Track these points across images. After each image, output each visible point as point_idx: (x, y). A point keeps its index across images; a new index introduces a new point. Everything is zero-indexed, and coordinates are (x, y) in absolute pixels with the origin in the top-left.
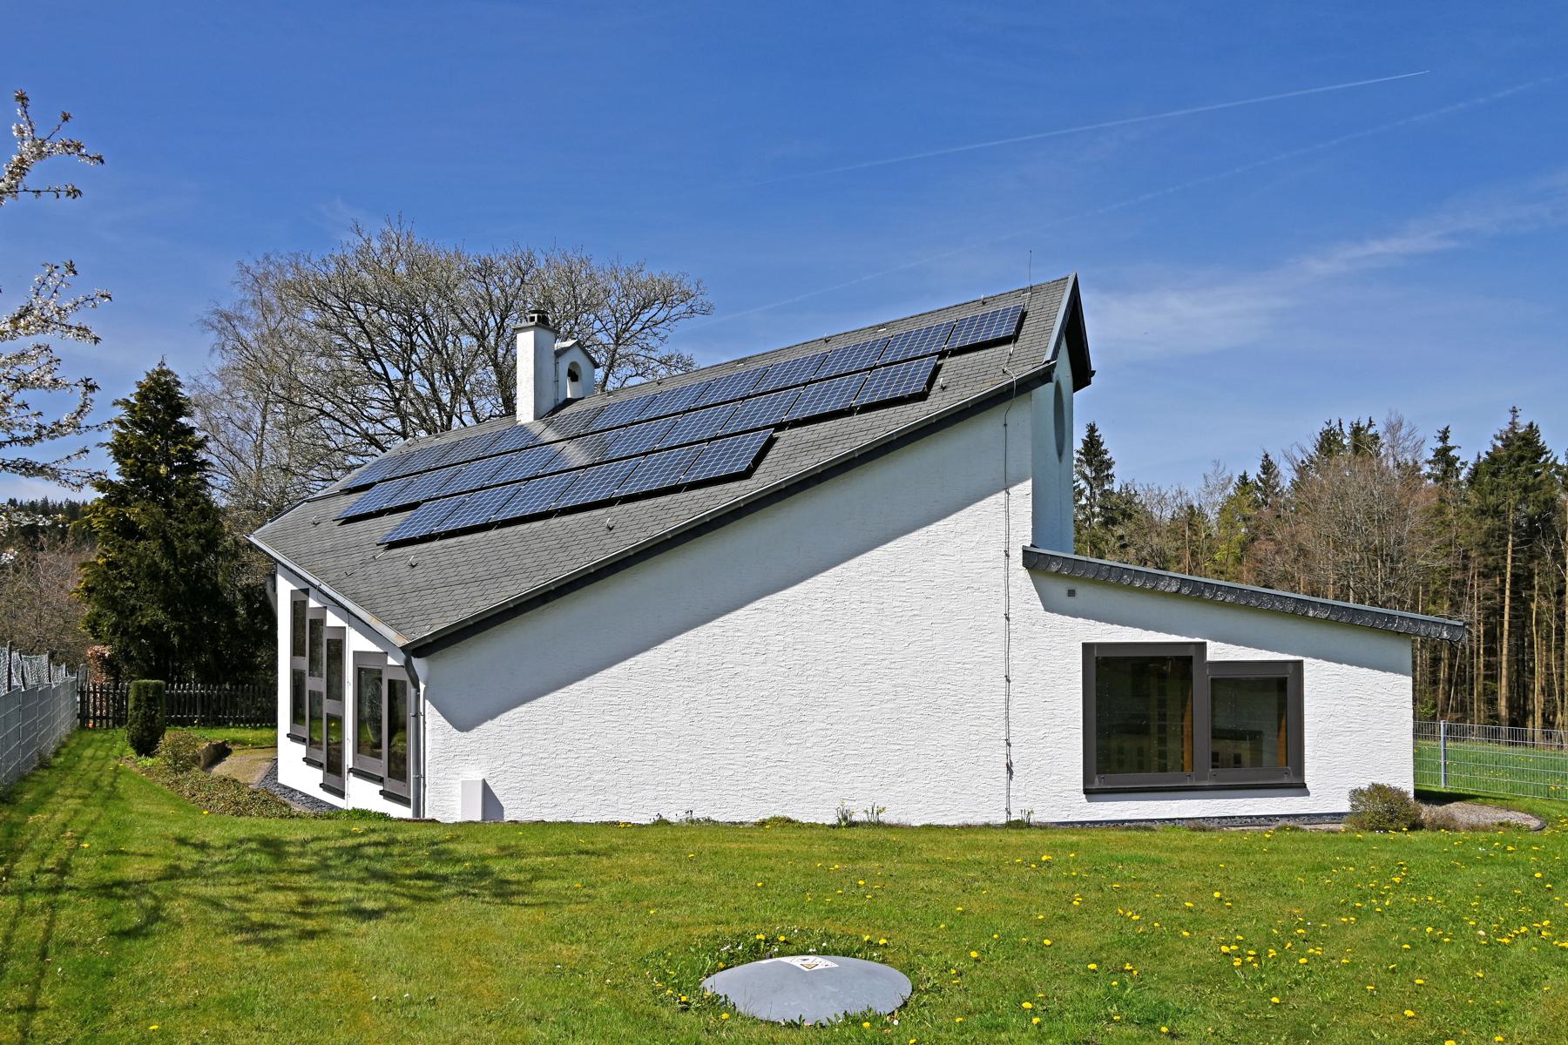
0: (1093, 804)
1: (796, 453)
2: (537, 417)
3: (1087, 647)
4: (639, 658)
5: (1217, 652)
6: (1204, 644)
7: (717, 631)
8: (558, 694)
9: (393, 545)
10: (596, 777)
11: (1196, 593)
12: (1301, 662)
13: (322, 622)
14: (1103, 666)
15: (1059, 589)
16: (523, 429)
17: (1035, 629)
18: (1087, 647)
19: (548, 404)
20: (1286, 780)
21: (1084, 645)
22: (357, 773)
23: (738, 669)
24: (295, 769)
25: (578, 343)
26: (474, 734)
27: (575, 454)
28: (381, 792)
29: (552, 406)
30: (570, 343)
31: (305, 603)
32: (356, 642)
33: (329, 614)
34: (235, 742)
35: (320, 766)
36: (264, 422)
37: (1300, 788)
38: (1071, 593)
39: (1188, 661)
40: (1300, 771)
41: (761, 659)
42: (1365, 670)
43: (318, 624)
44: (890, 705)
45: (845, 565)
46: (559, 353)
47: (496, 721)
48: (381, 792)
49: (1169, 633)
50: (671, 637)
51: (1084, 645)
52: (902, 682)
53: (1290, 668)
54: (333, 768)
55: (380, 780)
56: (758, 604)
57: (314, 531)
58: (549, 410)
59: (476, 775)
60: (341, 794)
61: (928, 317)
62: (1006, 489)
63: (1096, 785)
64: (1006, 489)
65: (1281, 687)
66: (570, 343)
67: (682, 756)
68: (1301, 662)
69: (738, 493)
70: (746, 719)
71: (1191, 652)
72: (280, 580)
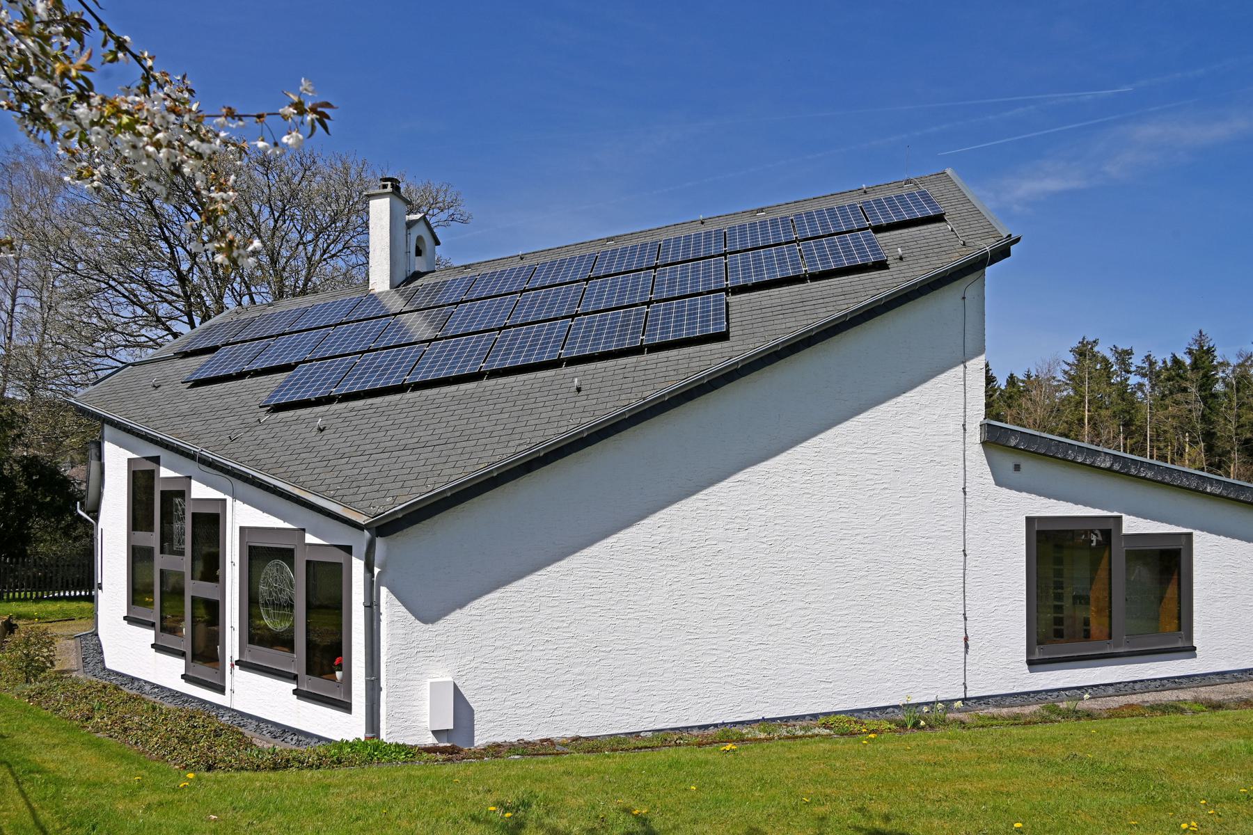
0: (1036, 675)
1: (760, 321)
2: (394, 286)
3: (1029, 520)
4: (620, 535)
5: (1132, 525)
6: (1120, 517)
7: (700, 504)
8: (534, 577)
9: (278, 408)
10: (576, 670)
11: (1123, 472)
12: (1191, 534)
13: (182, 494)
14: (1048, 542)
15: (1007, 461)
16: (374, 298)
17: (988, 503)
18: (1029, 520)
19: (401, 277)
20: (1180, 644)
21: (1027, 518)
22: (242, 664)
23: (721, 546)
24: (133, 650)
25: (424, 218)
26: (441, 625)
27: (418, 326)
28: (295, 692)
29: (404, 278)
30: (418, 216)
31: (151, 475)
32: (242, 516)
33: (194, 483)
34: (19, 617)
35: (182, 654)
36: (14, 305)
37: (1190, 651)
38: (1017, 468)
39: (1107, 534)
40: (1190, 636)
41: (743, 534)
42: (1236, 541)
43: (175, 496)
44: (864, 582)
45: (822, 436)
46: (410, 225)
47: (466, 609)
48: (295, 692)
49: (1103, 509)
50: (654, 512)
51: (1027, 518)
52: (864, 560)
53: (1184, 540)
54: (204, 655)
55: (293, 678)
56: (740, 476)
57: (156, 394)
58: (404, 280)
59: (445, 677)
60: (221, 690)
61: (807, 204)
62: (964, 362)
63: (1036, 657)
64: (964, 362)
65: (1169, 562)
66: (418, 216)
67: (665, 643)
68: (1191, 534)
69: (683, 364)
70: (729, 600)
71: (1110, 525)
72: (109, 449)
